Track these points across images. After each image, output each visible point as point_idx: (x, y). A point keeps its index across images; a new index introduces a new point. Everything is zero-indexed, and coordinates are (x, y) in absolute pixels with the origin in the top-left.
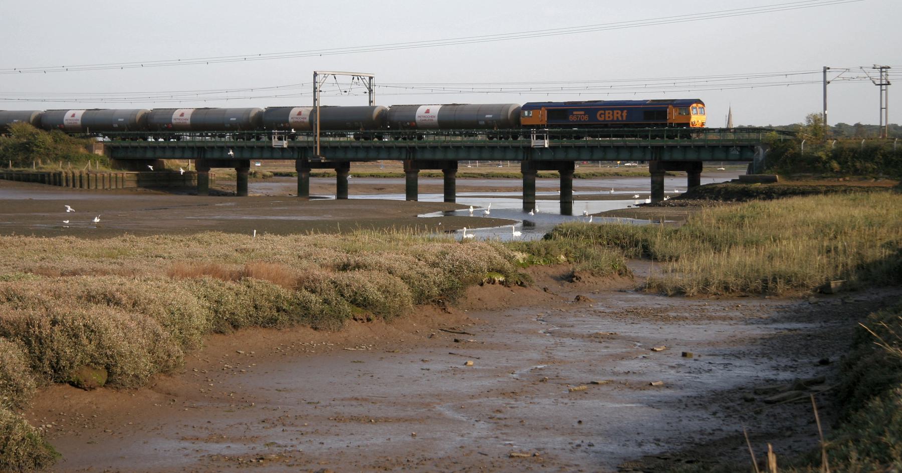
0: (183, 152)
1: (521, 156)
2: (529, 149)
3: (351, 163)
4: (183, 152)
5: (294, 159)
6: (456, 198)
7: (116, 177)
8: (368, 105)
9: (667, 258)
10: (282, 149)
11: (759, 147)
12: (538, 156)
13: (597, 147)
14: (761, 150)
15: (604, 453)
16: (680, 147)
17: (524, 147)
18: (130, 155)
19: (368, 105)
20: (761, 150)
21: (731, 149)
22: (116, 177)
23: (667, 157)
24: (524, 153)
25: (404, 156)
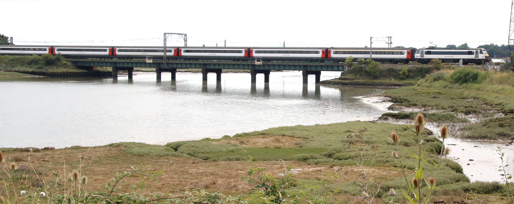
0: (107, 64)
1: (112, 65)
2: (254, 65)
3: (321, 71)
4: (107, 64)
5: (250, 70)
6: (118, 77)
7: (462, 129)
8: (184, 46)
9: (467, 88)
10: (150, 63)
11: (346, 66)
12: (257, 68)
13: (297, 65)
14: (346, 68)
15: (411, 119)
16: (303, 65)
17: (252, 65)
18: (84, 65)
19: (184, 46)
20: (346, 68)
21: (334, 67)
22: (462, 129)
23: (309, 69)
24: (252, 66)
25: (156, 66)
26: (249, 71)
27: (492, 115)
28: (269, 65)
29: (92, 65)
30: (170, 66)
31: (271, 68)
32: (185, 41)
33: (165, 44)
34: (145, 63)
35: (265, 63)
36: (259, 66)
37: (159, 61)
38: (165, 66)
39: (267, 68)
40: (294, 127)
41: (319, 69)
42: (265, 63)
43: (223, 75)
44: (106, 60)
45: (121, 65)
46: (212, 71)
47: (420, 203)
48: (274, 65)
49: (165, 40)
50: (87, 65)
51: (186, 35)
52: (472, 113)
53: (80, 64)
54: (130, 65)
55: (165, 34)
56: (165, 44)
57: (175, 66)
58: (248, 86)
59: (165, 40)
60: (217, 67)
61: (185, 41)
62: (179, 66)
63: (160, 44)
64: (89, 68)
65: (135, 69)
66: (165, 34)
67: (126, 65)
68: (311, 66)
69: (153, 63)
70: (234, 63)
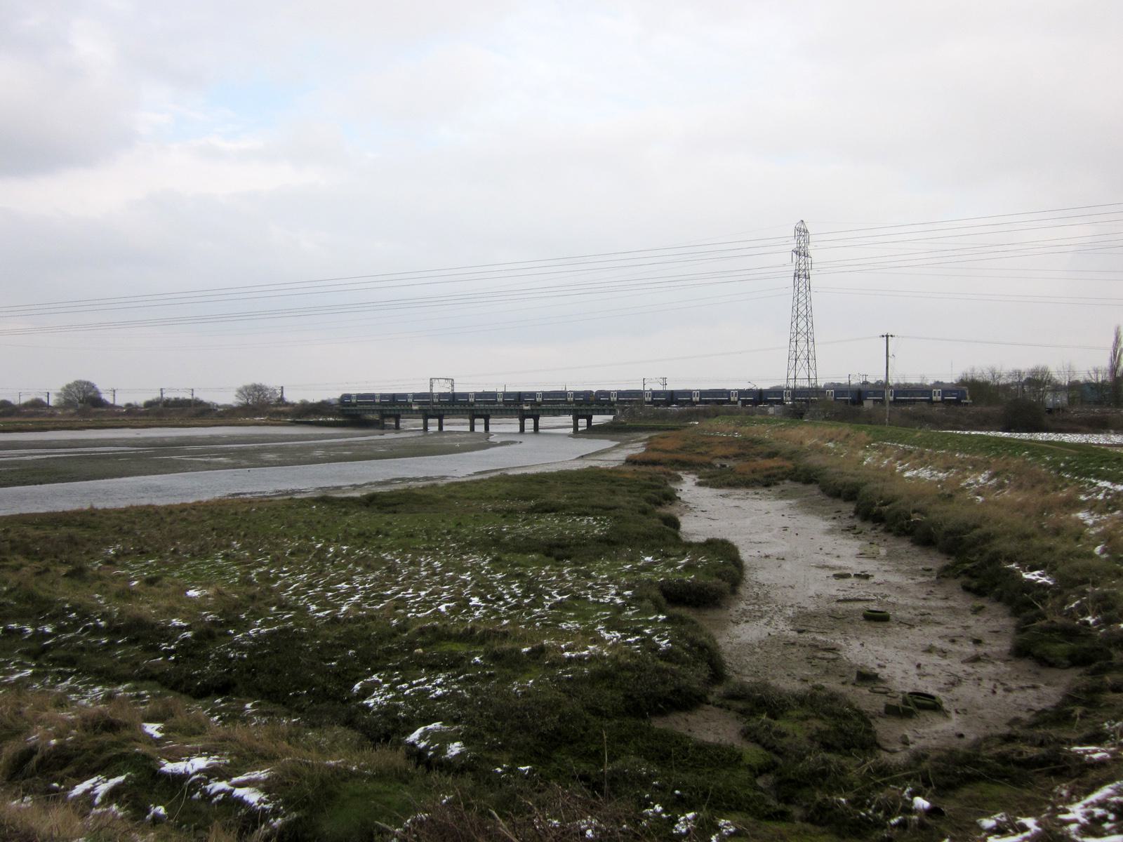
2: (523, 410)
10: (416, 410)
12: (525, 413)
23: (579, 413)
26: (468, 416)
27: (549, 779)
28: (538, 410)
29: (359, 413)
30: (437, 413)
31: (446, 412)
32: (453, 386)
33: (431, 390)
34: (412, 410)
35: (534, 407)
36: (528, 410)
37: (425, 407)
38: (432, 413)
39: (535, 413)
40: (555, 473)
41: (590, 413)
42: (534, 407)
43: (491, 421)
44: (512, 407)
45: (388, 413)
46: (480, 417)
47: (240, 836)
48: (543, 410)
49: (431, 386)
50: (354, 413)
51: (453, 380)
52: (231, 825)
53: (347, 413)
54: (397, 413)
55: (431, 379)
56: (431, 390)
57: (441, 413)
58: (517, 429)
59: (431, 386)
60: (484, 413)
61: (453, 386)
62: (494, 412)
63: (426, 389)
64: (357, 416)
65: (402, 416)
66: (431, 379)
67: (393, 413)
68: (581, 410)
69: (420, 410)
70: (463, 407)
